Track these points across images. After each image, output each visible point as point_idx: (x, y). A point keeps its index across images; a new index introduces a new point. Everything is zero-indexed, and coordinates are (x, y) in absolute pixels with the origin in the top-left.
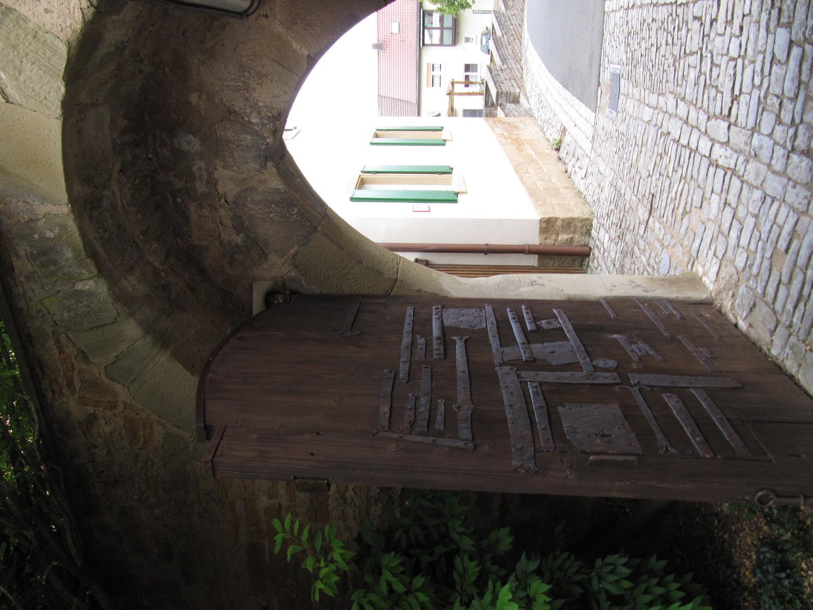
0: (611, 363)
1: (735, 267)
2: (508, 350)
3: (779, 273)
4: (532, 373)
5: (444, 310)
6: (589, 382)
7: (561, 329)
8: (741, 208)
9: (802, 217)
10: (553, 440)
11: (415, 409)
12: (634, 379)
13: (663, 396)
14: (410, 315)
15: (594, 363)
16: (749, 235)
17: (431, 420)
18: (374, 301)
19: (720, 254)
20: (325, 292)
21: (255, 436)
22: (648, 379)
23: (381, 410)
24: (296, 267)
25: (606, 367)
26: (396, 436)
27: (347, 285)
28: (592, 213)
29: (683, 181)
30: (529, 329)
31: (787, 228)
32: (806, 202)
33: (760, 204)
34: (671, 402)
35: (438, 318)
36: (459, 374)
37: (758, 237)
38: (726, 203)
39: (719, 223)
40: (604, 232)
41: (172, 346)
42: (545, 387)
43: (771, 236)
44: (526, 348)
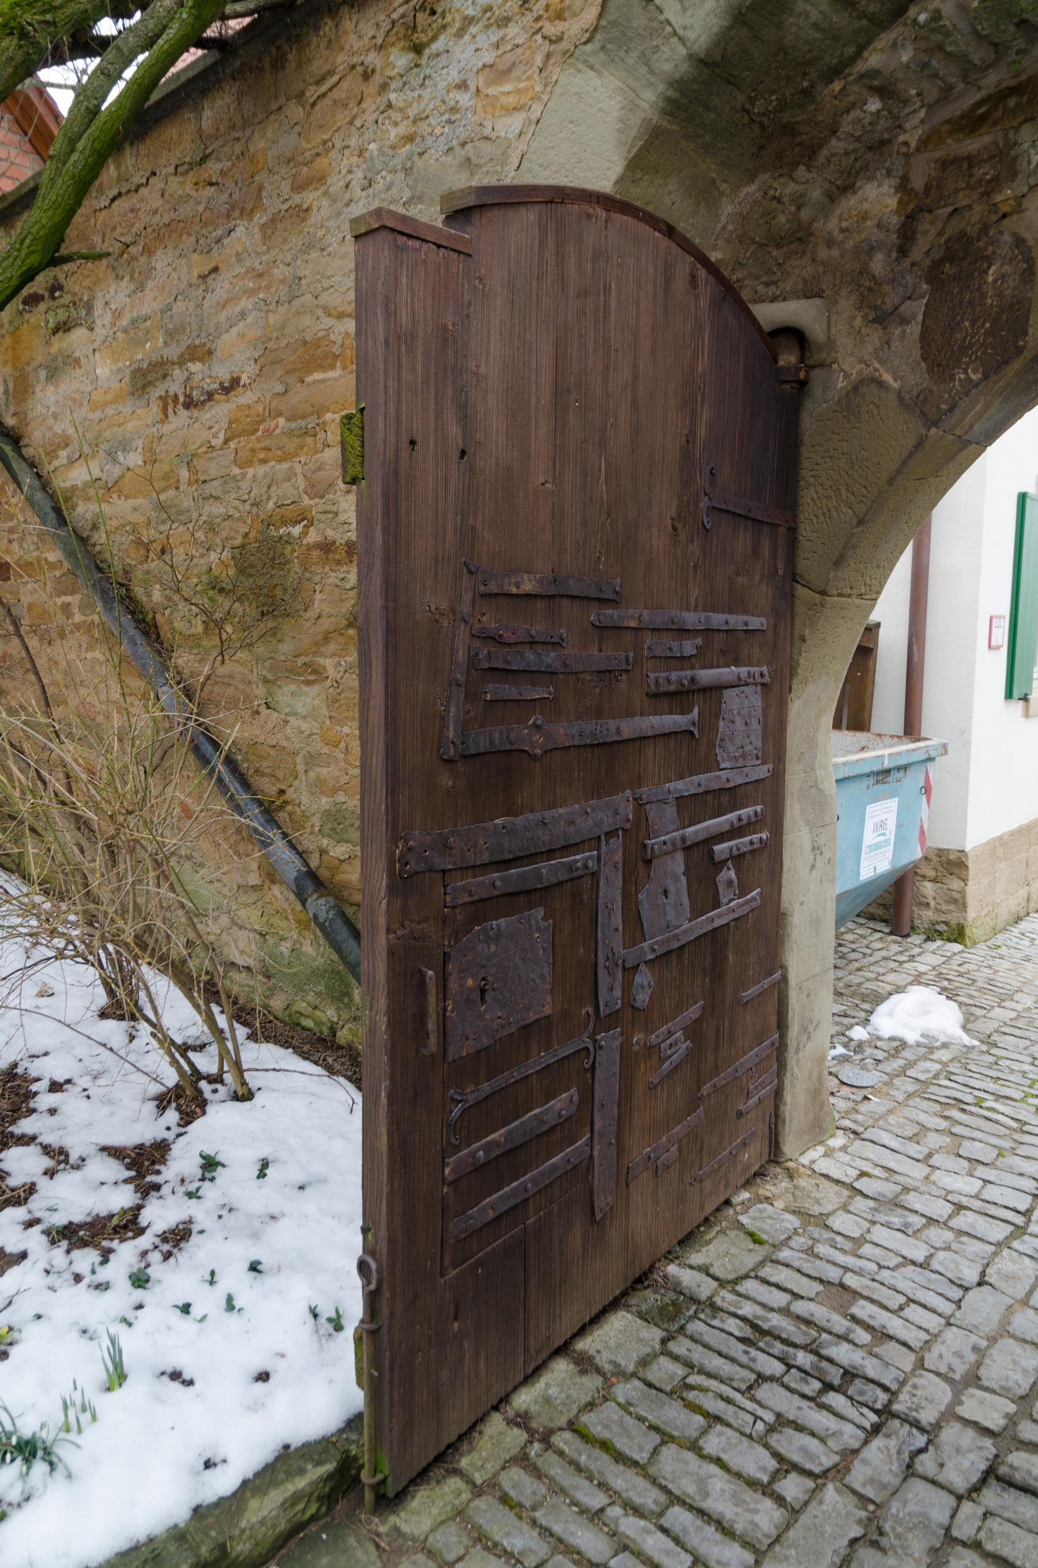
0: (642, 998)
1: (834, 1211)
2: (670, 811)
3: (813, 1295)
4: (618, 856)
5: (759, 689)
6: (601, 959)
7: (717, 905)
8: (949, 1236)
9: (912, 1357)
10: (471, 903)
11: (531, 643)
12: (610, 1040)
13: (573, 1090)
14: (746, 624)
15: (642, 967)
16: (890, 1246)
17: (505, 673)
18: (781, 553)
19: (861, 1185)
20: (805, 452)
21: (449, 320)
22: (608, 1065)
23: (525, 576)
24: (855, 388)
25: (634, 989)
26: (466, 609)
27: (815, 496)
28: (975, 943)
29: (1014, 1125)
30: (717, 848)
31: (895, 1325)
32: (943, 1370)
33: (949, 1275)
34: (562, 1103)
35: (739, 679)
36: (613, 724)
37: (885, 1264)
38: (960, 1207)
39: (923, 1189)
40: (935, 963)
41: (675, 127)
42: (587, 884)
43: (885, 1289)
44: (674, 845)
